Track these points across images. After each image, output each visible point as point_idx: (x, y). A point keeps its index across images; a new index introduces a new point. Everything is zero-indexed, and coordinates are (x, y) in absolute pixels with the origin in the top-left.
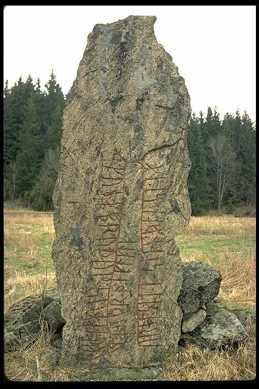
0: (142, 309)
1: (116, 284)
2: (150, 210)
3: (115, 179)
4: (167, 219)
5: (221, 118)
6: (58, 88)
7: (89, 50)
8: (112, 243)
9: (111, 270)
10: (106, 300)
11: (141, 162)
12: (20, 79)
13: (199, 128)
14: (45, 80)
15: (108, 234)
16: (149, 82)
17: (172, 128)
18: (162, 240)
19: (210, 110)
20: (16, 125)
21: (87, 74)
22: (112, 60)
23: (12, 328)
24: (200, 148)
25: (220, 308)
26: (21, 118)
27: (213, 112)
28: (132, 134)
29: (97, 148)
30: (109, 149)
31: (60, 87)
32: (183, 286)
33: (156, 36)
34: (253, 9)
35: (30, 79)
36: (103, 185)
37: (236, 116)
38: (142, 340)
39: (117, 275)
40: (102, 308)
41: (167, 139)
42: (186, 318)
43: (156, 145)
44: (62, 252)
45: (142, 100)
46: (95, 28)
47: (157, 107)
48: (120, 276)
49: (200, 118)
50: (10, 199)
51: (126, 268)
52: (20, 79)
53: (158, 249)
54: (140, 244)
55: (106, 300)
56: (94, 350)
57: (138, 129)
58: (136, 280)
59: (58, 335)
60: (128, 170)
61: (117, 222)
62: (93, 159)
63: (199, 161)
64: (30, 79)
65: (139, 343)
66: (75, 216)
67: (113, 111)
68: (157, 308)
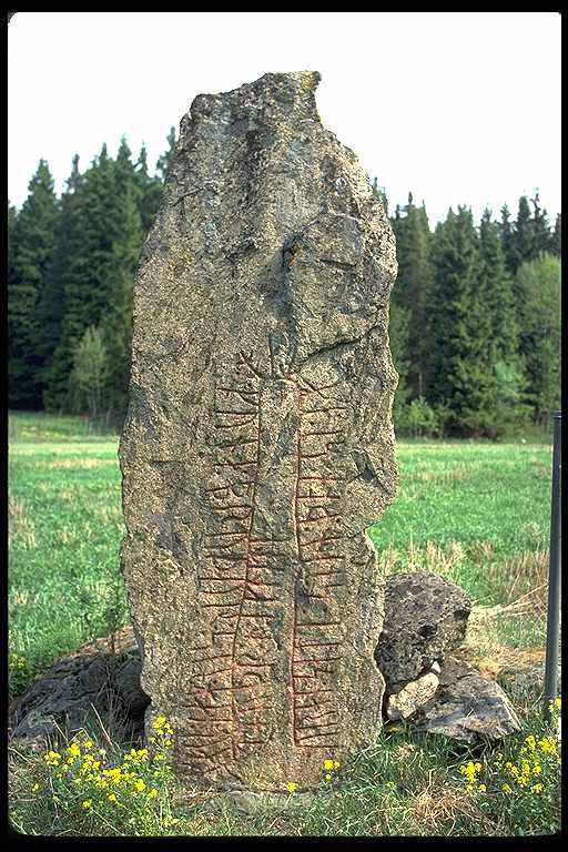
0: (300, 674)
2: (313, 475)
3: (240, 413)
4: (349, 492)
10: (228, 655)
11: (293, 376)
12: (104, 152)
13: (500, 244)
16: (306, 212)
18: (339, 535)
19: (523, 203)
20: (97, 253)
21: (182, 199)
22: (231, 168)
24: (502, 290)
25: (470, 670)
27: (532, 209)
30: (229, 351)
32: (386, 625)
34: (554, 19)
35: (124, 152)
36: (218, 427)
38: (302, 736)
40: (220, 671)
41: (345, 330)
42: (393, 687)
45: (292, 252)
46: (194, 105)
49: (502, 222)
50: (90, 414)
51: (267, 591)
52: (104, 152)
53: (332, 553)
54: (294, 544)
55: (228, 655)
57: (287, 311)
58: (288, 613)
59: (134, 725)
60: (267, 395)
61: (247, 500)
62: (196, 374)
63: (500, 320)
64: (124, 152)
65: (297, 741)
66: (163, 489)
67: (233, 275)
68: (331, 672)
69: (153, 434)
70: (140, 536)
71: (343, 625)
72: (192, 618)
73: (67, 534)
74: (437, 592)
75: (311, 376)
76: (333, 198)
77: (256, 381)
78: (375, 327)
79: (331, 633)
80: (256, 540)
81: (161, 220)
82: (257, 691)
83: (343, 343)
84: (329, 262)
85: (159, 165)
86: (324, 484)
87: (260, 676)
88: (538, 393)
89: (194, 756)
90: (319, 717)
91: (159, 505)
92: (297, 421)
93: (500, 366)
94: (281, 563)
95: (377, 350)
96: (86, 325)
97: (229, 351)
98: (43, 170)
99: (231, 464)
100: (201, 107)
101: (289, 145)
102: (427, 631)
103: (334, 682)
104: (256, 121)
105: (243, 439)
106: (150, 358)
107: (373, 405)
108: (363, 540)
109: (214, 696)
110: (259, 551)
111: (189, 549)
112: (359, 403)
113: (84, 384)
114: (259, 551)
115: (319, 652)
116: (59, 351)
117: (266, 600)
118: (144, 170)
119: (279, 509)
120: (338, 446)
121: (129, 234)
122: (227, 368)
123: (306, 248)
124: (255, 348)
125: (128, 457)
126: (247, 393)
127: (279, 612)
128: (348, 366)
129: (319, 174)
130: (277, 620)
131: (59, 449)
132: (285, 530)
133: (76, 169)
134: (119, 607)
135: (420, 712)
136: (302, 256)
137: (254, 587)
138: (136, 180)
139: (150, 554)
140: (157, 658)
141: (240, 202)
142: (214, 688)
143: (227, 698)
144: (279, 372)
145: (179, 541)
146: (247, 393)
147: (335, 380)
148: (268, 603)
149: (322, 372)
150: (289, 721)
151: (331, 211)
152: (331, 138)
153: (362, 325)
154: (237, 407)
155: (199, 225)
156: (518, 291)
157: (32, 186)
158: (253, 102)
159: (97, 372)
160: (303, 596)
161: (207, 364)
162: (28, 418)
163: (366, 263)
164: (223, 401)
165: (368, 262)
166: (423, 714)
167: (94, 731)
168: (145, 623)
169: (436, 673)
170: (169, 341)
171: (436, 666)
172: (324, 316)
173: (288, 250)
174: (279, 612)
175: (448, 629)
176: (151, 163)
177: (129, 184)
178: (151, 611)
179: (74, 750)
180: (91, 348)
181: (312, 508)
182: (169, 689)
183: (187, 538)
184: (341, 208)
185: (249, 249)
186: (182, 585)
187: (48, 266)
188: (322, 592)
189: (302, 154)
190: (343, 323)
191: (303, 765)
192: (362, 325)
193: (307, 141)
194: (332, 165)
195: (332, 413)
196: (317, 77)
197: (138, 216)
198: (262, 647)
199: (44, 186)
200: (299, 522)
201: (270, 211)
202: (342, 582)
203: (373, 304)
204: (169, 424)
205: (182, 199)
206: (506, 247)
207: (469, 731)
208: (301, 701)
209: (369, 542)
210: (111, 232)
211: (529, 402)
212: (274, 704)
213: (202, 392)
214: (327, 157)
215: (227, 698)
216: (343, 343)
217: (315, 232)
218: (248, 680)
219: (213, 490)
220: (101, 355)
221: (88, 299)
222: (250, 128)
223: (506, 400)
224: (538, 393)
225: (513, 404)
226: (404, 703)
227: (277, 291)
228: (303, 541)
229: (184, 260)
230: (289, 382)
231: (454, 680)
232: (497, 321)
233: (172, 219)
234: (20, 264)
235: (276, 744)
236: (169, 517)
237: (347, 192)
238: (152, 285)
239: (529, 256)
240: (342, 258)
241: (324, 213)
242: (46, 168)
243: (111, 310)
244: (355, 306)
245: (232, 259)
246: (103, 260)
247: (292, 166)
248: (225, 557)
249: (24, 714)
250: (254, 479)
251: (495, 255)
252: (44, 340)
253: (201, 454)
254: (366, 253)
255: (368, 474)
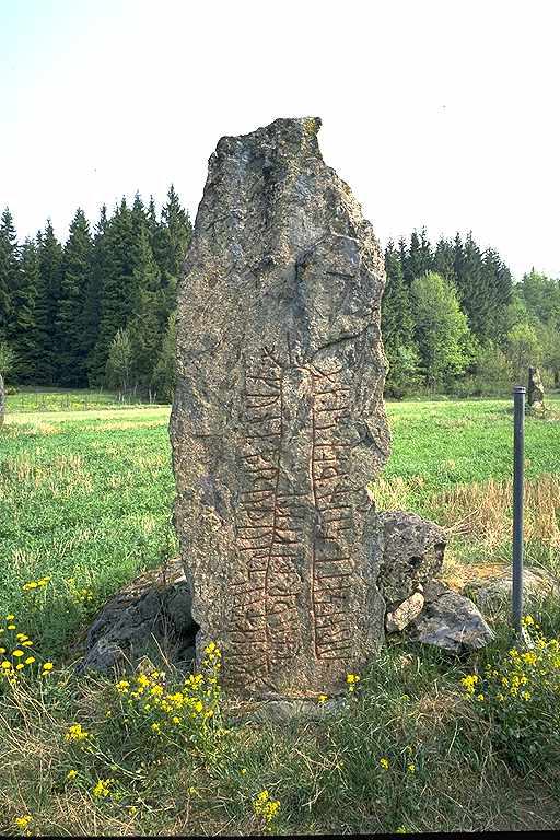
2: (325, 442)
5: (433, 249)
6: (182, 216)
7: (212, 184)
12: (124, 204)
14: (162, 201)
16: (313, 234)
17: (355, 309)
19: (414, 237)
20: (123, 277)
23: (116, 636)
26: (131, 266)
27: (420, 241)
28: (291, 320)
30: (254, 347)
33: (322, 152)
35: (138, 204)
36: (248, 407)
37: (454, 244)
44: (188, 516)
45: (304, 266)
46: (219, 145)
50: (122, 389)
52: (124, 204)
53: (341, 503)
54: (311, 497)
57: (301, 313)
60: (287, 380)
64: (138, 204)
69: (197, 413)
70: (189, 496)
71: (352, 560)
72: (232, 560)
73: (114, 480)
74: (418, 528)
75: (321, 365)
76: (334, 222)
77: (277, 370)
78: (370, 325)
79: (342, 566)
80: (281, 495)
81: (197, 242)
82: (285, 616)
83: (345, 338)
84: (334, 274)
85: (163, 214)
86: (333, 449)
87: (288, 604)
88: (427, 367)
89: (237, 671)
90: (335, 635)
91: (202, 471)
92: (311, 401)
93: (401, 349)
94: (300, 513)
95: (373, 344)
96: (117, 328)
97: (254, 347)
98: (80, 216)
99: (259, 436)
100: (225, 146)
101: (298, 179)
102: (415, 561)
103: (346, 605)
104: (271, 159)
105: (269, 416)
106: (190, 354)
107: (371, 386)
108: (366, 492)
109: (251, 622)
110: (284, 504)
111: (228, 504)
112: (359, 385)
113: (117, 369)
114: (284, 504)
115: (333, 582)
116: (98, 345)
117: (291, 542)
118: (152, 218)
119: (299, 470)
120: (344, 419)
121: (144, 263)
122: (253, 360)
123: (314, 263)
124: (275, 343)
125: (176, 429)
126: (271, 380)
127: (301, 552)
128: (350, 356)
129: (323, 203)
130: (299, 558)
131: (102, 414)
132: (303, 487)
133: (104, 217)
134: (169, 548)
135: (411, 625)
136: (312, 269)
137: (281, 533)
138: (148, 225)
139: (197, 509)
140: (204, 593)
141: (260, 226)
142: (252, 615)
143: (262, 623)
144: (296, 363)
145: (220, 499)
146: (271, 380)
147: (340, 368)
148: (292, 545)
149: (330, 363)
150: (312, 639)
151: (334, 233)
152: (332, 173)
153: (361, 323)
154: (263, 391)
155: (228, 245)
156: (413, 298)
157: (73, 228)
158: (267, 143)
159: (126, 359)
160: (319, 538)
161: (238, 358)
162: (77, 394)
163: (362, 274)
164: (251, 384)
165: (364, 273)
166: (415, 626)
167: (159, 663)
168: (194, 566)
169: (421, 592)
170: (207, 339)
171: (420, 587)
172: (330, 317)
173: (300, 266)
174: (301, 552)
175: (430, 558)
176: (158, 211)
177: (143, 227)
178: (199, 556)
179: (143, 680)
180: (121, 343)
181: (325, 469)
182: (215, 618)
183: (226, 495)
184: (340, 230)
185: (268, 265)
186: (223, 533)
187: (88, 286)
188: (335, 535)
189: (309, 187)
190: (346, 322)
191: (324, 673)
192: (361, 323)
193: (313, 175)
194: (333, 195)
195: (338, 393)
196: (318, 122)
197: (150, 250)
198: (288, 580)
199: (81, 229)
200: (315, 480)
201: (285, 233)
202: (351, 525)
203: (369, 306)
204: (209, 406)
205: (213, 224)
206: (404, 268)
207: (456, 642)
208: (321, 622)
209: (370, 494)
210: (132, 262)
211: (422, 373)
212: (300, 625)
213: (236, 378)
214: (329, 188)
215: (262, 623)
216: (345, 338)
217: (321, 250)
218: (278, 607)
219: (245, 458)
220: (128, 348)
221: (118, 309)
222: (266, 165)
223: (406, 372)
224: (427, 367)
225: (411, 375)
226: (400, 619)
227: (292, 299)
228: (319, 495)
229: (217, 275)
230: (304, 370)
231: (436, 597)
232: (399, 318)
233: (205, 241)
234: (67, 285)
235: (302, 658)
236: (211, 479)
237: (345, 217)
238: (191, 295)
239: (419, 273)
240: (344, 271)
241: (329, 234)
242: (83, 217)
243: (134, 316)
244: (355, 309)
245: (256, 273)
246: (128, 282)
247: (301, 197)
248: (257, 509)
249: (95, 640)
250: (277, 445)
251: (396, 274)
252: (88, 338)
253: (235, 429)
254: (363, 266)
255: (368, 440)
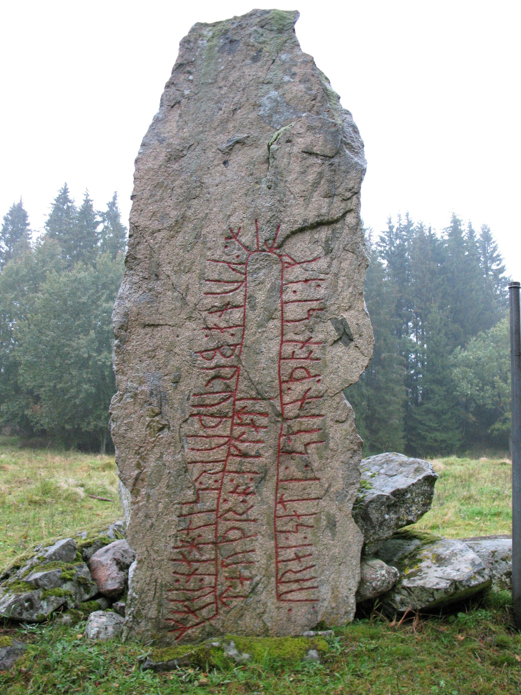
1: (232, 480)
8: (225, 400)
9: (220, 454)
15: (218, 385)
29: (195, 229)
31: (78, 204)
39: (233, 464)
43: (305, 221)
47: (305, 155)
48: (241, 464)
56: (189, 609)
